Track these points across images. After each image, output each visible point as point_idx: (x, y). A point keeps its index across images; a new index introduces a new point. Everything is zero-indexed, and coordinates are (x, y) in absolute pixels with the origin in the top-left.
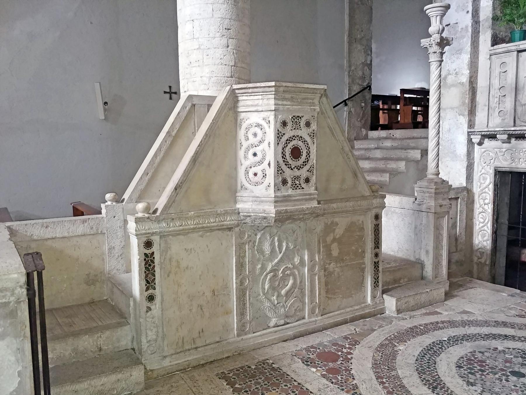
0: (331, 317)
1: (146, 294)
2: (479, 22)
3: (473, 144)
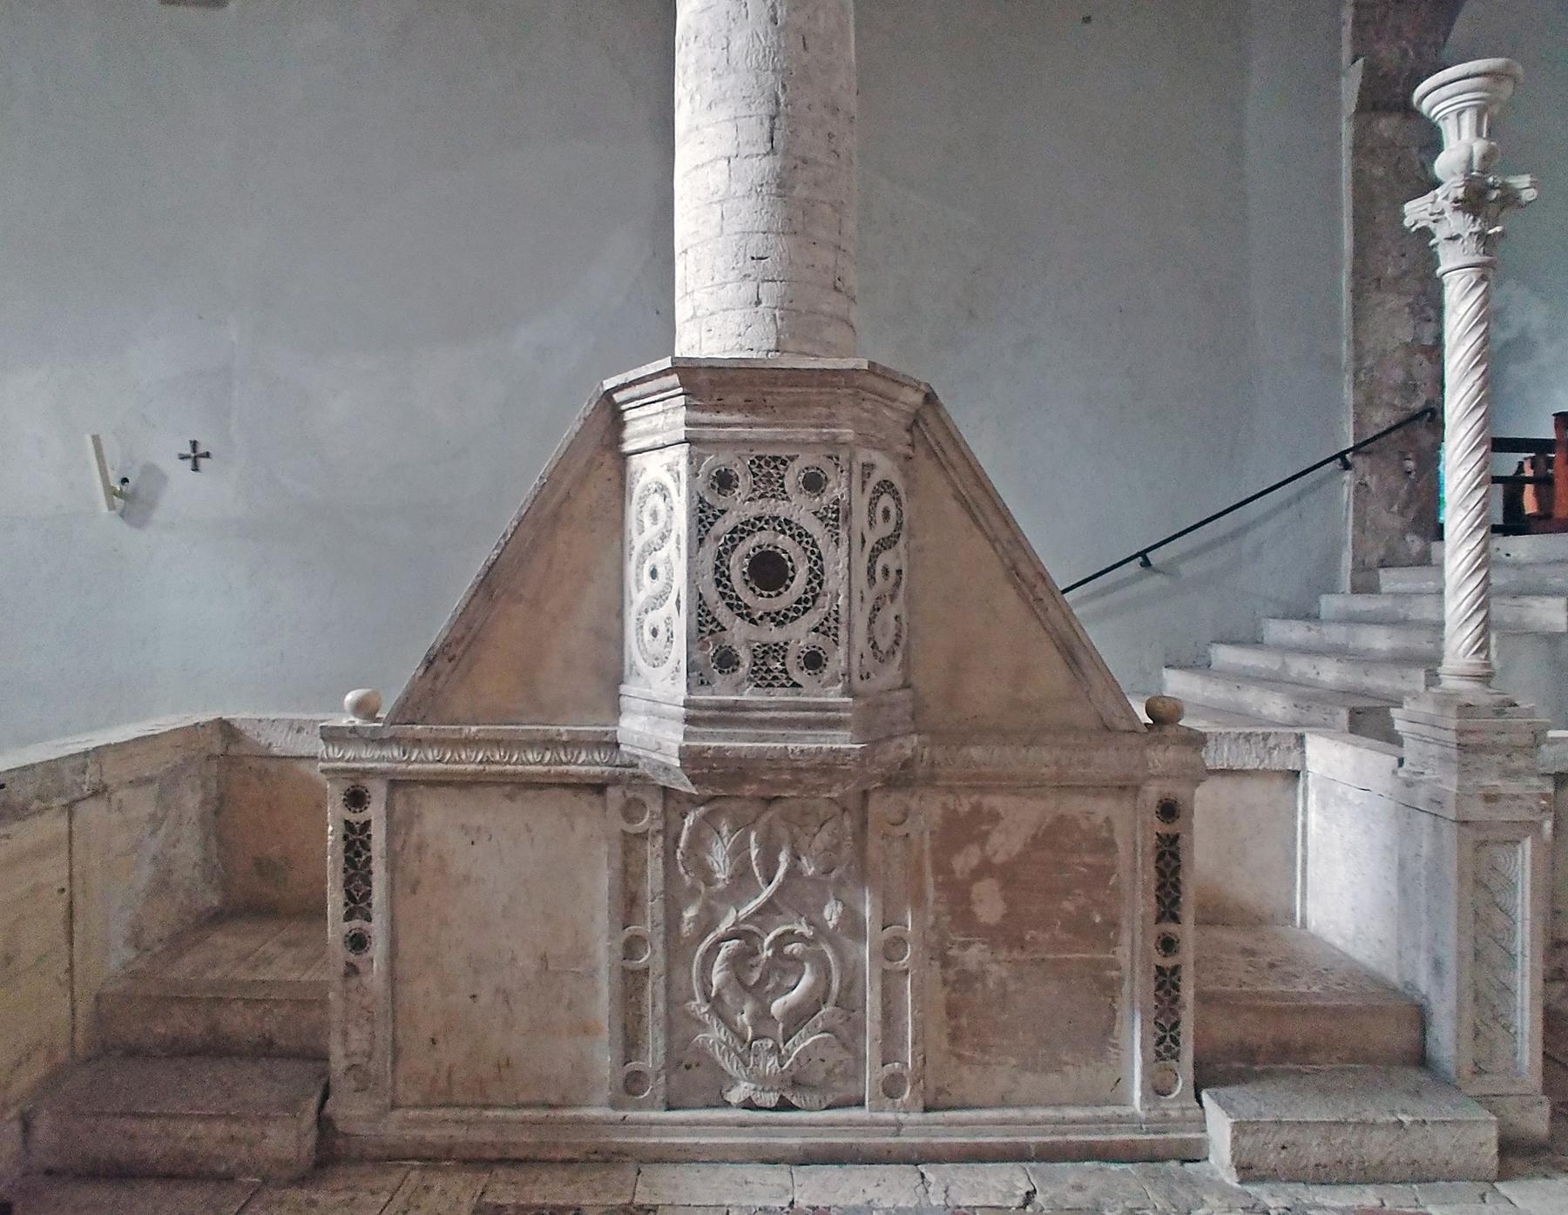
0: (960, 1124)
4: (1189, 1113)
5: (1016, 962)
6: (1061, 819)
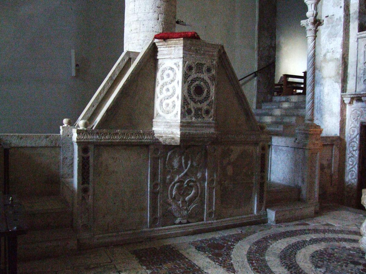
1: (82, 186)
2: (350, 15)
3: (345, 104)
4: (265, 214)
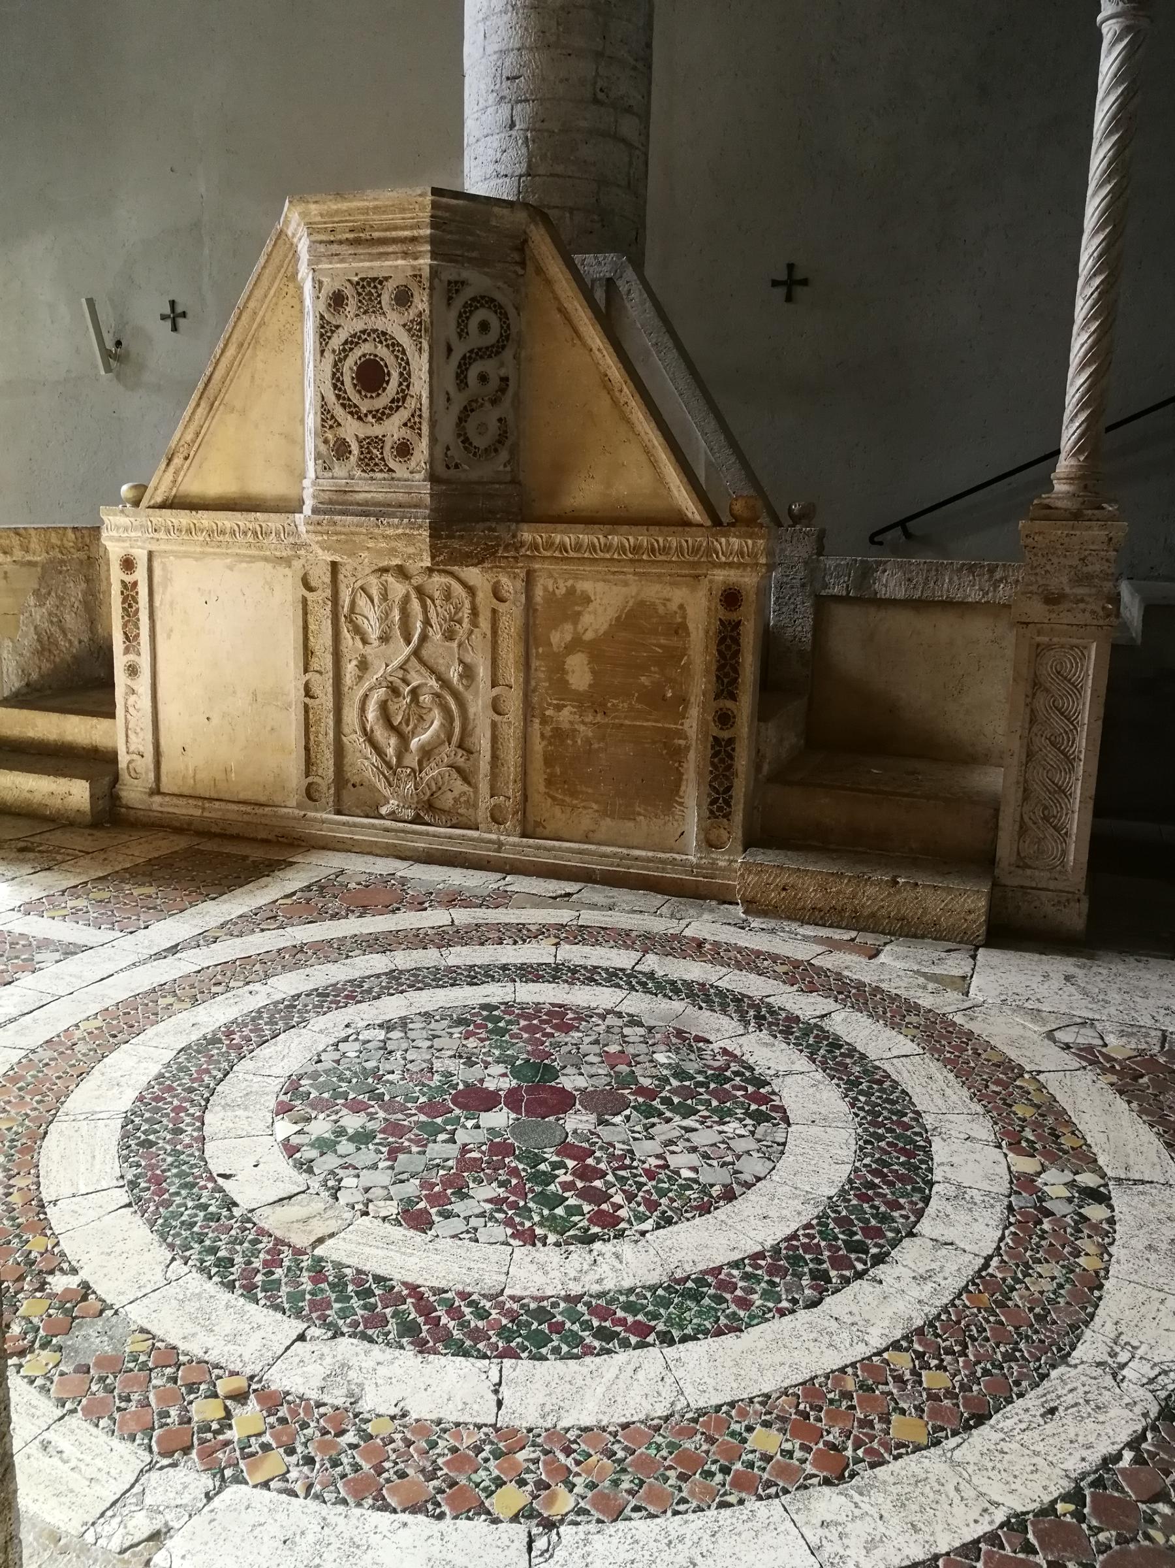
5: (599, 726)
6: (642, 603)
